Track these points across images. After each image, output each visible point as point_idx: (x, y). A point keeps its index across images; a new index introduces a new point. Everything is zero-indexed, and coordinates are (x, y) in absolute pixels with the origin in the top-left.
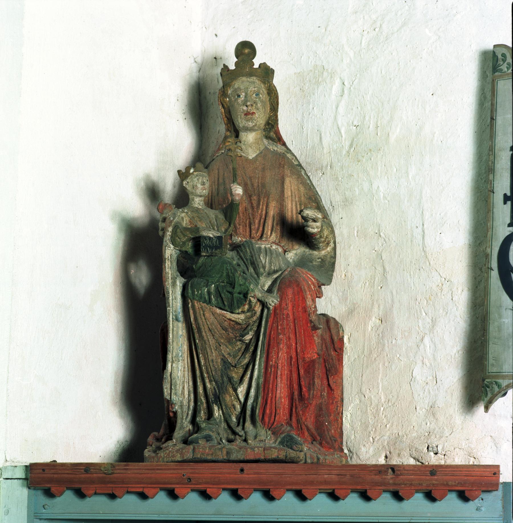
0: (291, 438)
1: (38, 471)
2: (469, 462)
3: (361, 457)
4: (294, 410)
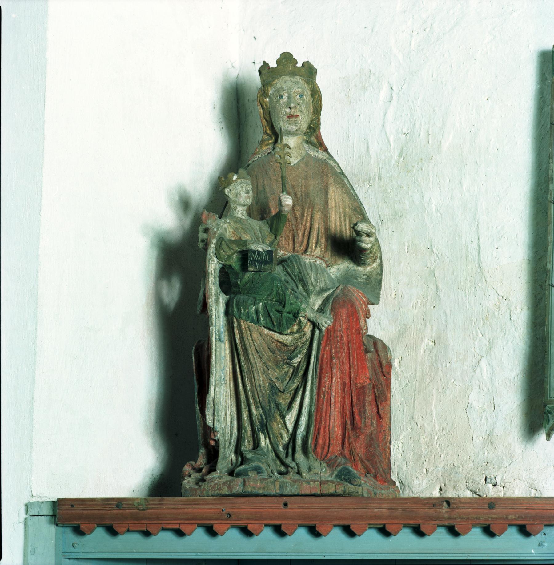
1: (66, 507)
3: (413, 490)
4: (346, 440)
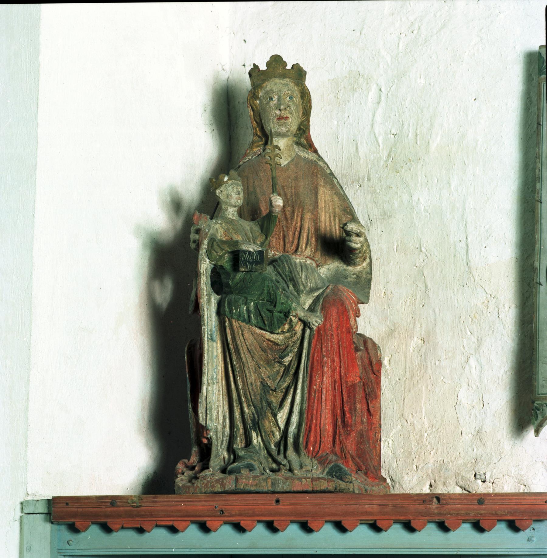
0: (340, 469)
2: (519, 490)
3: (404, 486)
4: (337, 438)
